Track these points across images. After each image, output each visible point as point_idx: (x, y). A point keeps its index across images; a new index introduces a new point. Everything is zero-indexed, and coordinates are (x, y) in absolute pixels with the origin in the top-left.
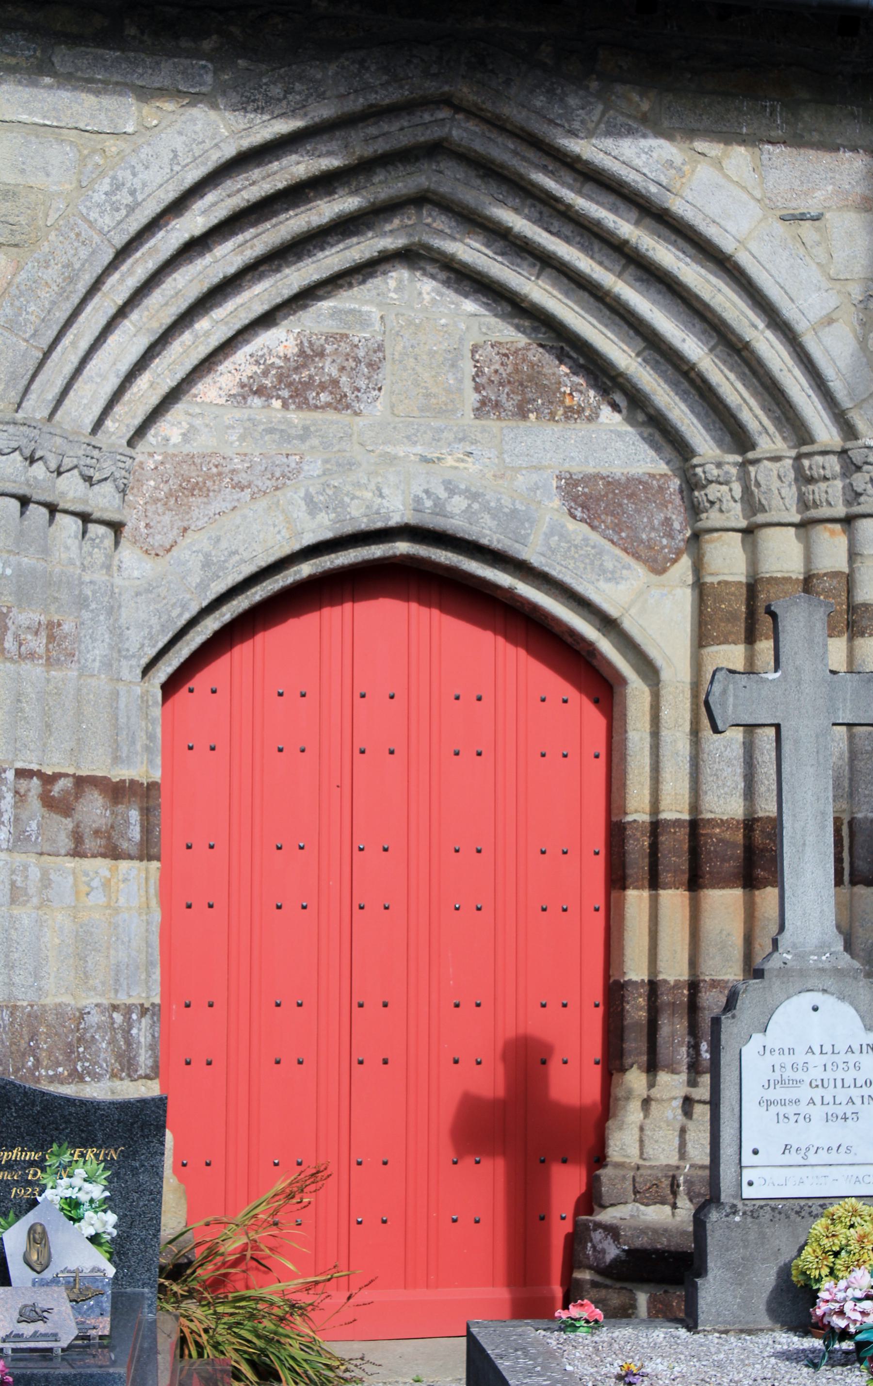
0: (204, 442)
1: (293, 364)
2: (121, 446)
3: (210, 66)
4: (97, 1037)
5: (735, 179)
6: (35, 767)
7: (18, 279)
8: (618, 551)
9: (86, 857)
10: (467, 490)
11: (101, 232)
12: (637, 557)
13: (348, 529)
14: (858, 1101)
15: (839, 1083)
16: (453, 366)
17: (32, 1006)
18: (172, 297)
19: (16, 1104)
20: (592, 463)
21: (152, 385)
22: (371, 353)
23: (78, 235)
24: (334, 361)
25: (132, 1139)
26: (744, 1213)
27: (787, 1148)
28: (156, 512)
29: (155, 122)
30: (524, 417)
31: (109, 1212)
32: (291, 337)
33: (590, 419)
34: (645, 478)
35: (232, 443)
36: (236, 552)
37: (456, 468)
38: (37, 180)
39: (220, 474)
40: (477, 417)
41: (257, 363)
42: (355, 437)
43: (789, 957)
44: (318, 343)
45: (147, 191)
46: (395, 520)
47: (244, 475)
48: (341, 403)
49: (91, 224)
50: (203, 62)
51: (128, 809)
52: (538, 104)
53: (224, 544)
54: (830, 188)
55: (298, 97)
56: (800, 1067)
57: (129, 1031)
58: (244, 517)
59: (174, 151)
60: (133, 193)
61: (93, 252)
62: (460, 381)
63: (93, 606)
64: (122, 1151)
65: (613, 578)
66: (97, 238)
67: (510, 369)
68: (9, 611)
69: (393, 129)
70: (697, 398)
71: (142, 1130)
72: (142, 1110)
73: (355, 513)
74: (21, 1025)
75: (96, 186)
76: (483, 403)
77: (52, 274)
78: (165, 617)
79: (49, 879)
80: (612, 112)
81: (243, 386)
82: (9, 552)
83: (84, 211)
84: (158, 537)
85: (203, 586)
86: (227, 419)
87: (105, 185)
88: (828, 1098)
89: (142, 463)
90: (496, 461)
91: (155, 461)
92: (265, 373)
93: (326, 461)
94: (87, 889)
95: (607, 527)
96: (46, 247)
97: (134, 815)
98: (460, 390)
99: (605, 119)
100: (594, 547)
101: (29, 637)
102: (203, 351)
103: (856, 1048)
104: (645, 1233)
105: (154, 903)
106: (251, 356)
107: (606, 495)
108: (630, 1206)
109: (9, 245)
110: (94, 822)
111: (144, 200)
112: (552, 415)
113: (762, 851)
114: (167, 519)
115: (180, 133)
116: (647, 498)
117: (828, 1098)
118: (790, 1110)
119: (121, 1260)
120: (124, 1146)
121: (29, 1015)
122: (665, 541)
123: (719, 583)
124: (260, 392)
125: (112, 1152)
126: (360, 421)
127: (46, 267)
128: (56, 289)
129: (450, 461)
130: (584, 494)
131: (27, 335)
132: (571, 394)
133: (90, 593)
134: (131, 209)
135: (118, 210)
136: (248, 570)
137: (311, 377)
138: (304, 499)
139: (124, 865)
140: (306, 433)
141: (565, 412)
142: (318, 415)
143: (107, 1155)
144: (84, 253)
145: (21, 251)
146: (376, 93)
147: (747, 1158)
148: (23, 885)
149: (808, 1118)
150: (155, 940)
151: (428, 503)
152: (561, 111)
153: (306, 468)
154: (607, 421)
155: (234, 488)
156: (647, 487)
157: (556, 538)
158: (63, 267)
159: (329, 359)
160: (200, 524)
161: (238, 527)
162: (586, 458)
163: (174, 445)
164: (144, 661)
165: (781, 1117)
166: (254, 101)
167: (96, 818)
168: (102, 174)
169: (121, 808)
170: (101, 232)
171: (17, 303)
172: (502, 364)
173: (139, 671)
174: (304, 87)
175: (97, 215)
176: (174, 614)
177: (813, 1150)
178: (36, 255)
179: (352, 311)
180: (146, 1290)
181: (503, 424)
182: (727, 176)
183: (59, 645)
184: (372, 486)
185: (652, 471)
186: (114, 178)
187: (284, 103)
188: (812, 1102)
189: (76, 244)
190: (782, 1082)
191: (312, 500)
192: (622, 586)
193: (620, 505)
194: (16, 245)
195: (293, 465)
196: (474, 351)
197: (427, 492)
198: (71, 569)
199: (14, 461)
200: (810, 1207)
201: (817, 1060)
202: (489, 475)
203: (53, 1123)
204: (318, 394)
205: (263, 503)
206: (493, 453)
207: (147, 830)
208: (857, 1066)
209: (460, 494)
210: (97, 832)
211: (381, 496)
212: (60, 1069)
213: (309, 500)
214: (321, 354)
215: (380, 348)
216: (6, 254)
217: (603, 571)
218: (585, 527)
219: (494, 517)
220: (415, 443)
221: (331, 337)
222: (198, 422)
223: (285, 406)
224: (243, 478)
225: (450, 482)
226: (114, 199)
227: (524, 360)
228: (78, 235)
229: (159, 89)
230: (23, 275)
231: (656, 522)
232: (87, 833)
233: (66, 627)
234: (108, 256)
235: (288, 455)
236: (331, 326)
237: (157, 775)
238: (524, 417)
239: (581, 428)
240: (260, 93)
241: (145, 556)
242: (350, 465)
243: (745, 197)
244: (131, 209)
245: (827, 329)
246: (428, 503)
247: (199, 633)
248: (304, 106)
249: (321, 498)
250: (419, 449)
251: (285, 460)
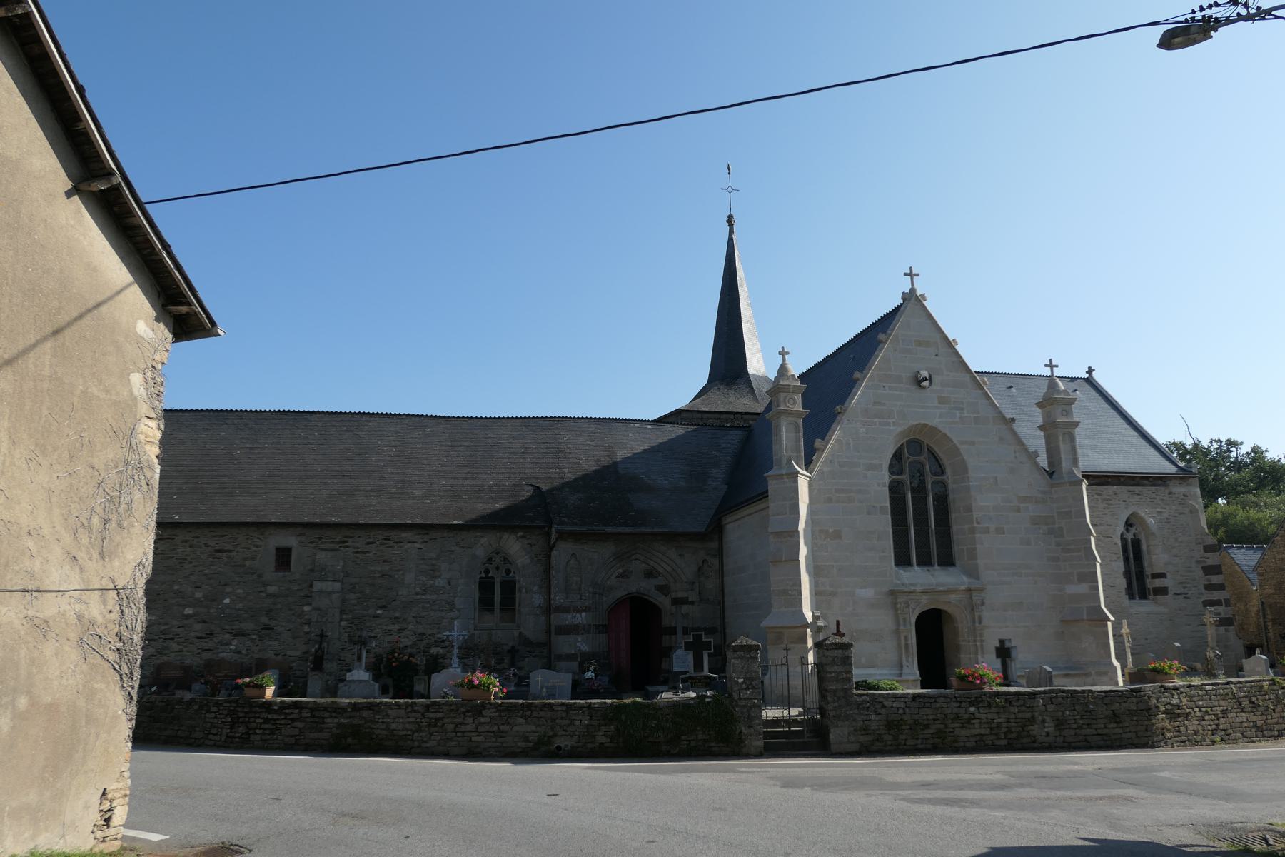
48: (628, 578)
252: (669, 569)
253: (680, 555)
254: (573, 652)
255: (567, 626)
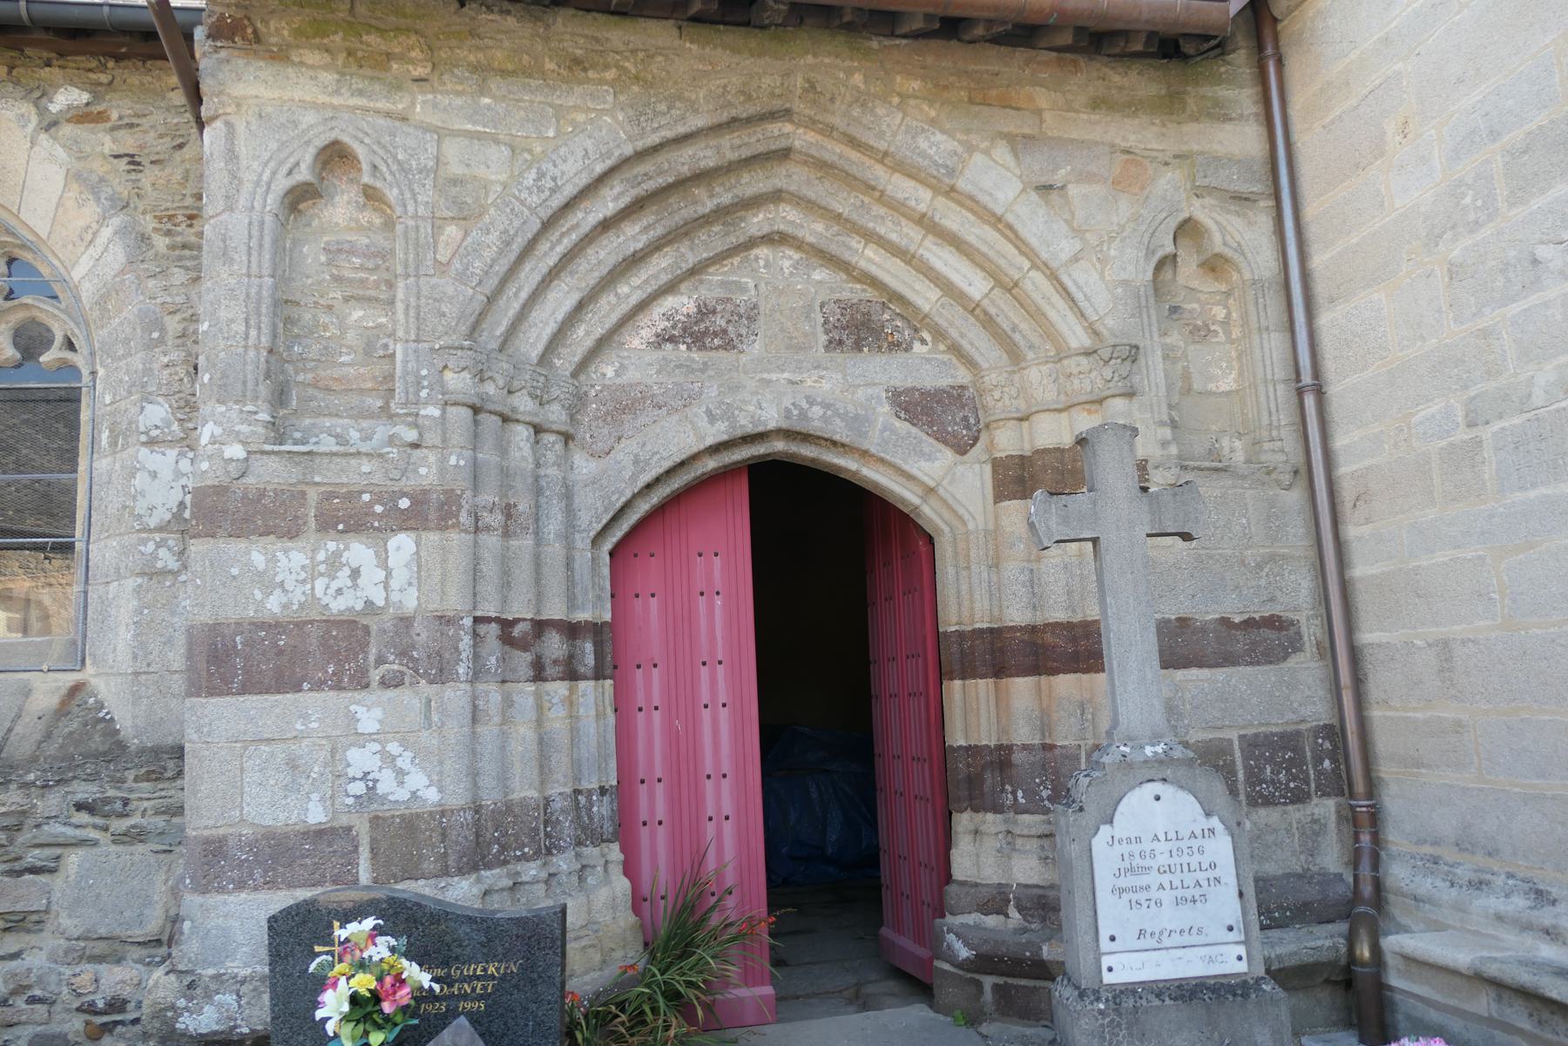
0: (632, 375)
1: (694, 320)
7: (465, 244)
8: (932, 440)
11: (529, 208)
12: (945, 442)
13: (739, 433)
14: (1205, 883)
15: (1185, 868)
19: (422, 924)
23: (512, 210)
26: (1107, 1000)
27: (1142, 933)
28: (597, 427)
30: (861, 350)
33: (906, 350)
36: (658, 452)
38: (481, 171)
41: (668, 320)
43: (1127, 750)
45: (565, 178)
46: (772, 425)
48: (728, 345)
49: (522, 203)
53: (648, 447)
54: (1069, 168)
58: (662, 427)
59: (586, 150)
60: (554, 179)
61: (524, 223)
63: (548, 493)
65: (930, 458)
66: (526, 212)
67: (848, 317)
73: (743, 422)
77: (493, 237)
78: (606, 502)
85: (634, 478)
86: (647, 359)
87: (533, 174)
88: (1177, 883)
92: (674, 327)
93: (720, 386)
94: (549, 705)
96: (487, 219)
97: (589, 647)
98: (814, 334)
102: (625, 308)
103: (1198, 832)
105: (610, 711)
108: (973, 915)
112: (880, 348)
117: (1177, 883)
118: (1142, 896)
121: (493, 811)
124: (672, 339)
129: (810, 383)
136: (667, 465)
137: (706, 328)
138: (706, 412)
140: (705, 367)
142: (713, 354)
144: (516, 223)
147: (1105, 944)
151: (795, 412)
164: (592, 534)
168: (529, 168)
169: (578, 642)
170: (529, 208)
176: (614, 498)
186: (538, 169)
188: (1161, 887)
190: (1131, 870)
192: (937, 464)
193: (932, 408)
194: (464, 219)
196: (822, 306)
197: (793, 404)
198: (524, 464)
199: (464, 379)
201: (1162, 847)
202: (837, 392)
205: (676, 417)
206: (839, 376)
208: (1201, 851)
210: (555, 662)
211: (761, 408)
212: (526, 850)
213: (709, 413)
215: (755, 306)
217: (922, 454)
219: (842, 420)
220: (783, 371)
221: (720, 300)
223: (689, 348)
224: (660, 400)
230: (469, 239)
232: (547, 662)
233: (520, 508)
234: (535, 225)
236: (720, 293)
238: (861, 350)
239: (900, 356)
243: (1009, 175)
244: (553, 191)
246: (795, 412)
250: (786, 375)
252: (976, 285)
253: (1045, 189)
254: (316, 815)
255: (275, 627)
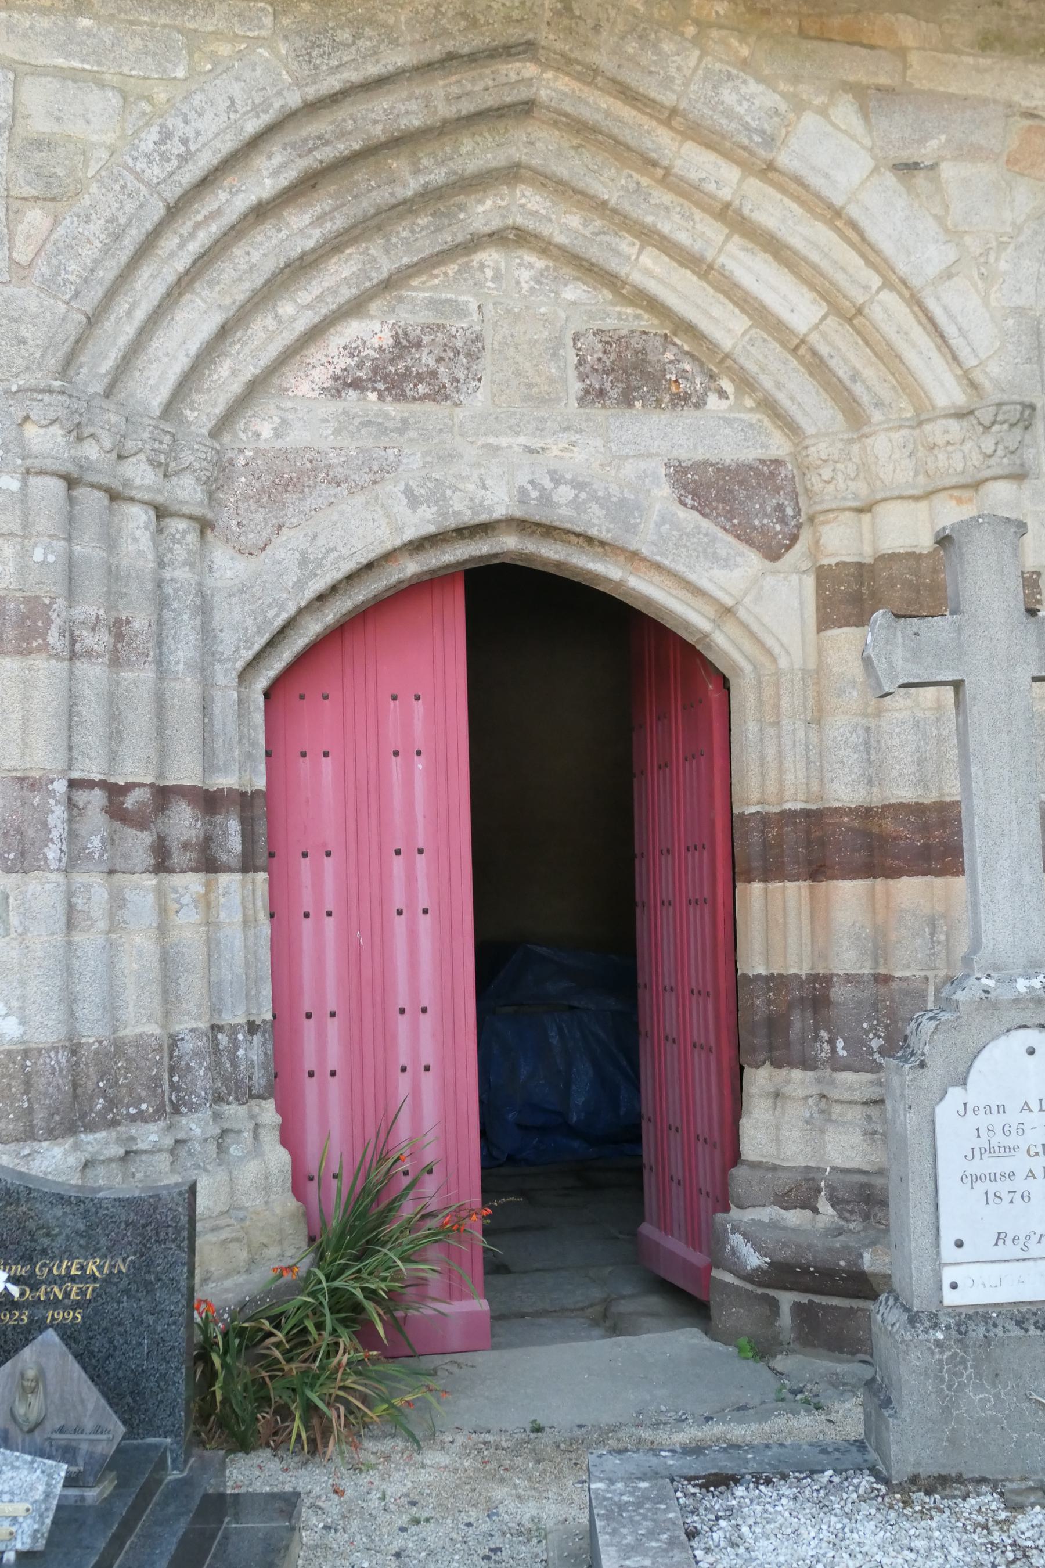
0: (297, 437)
1: (389, 356)
2: (202, 435)
3: (269, 8)
4: (193, 1064)
5: (843, 127)
6: (97, 777)
7: (54, 236)
8: (730, 538)
9: (175, 872)
10: (572, 481)
11: (148, 184)
12: (750, 542)
13: (452, 523)
16: (554, 354)
17: (100, 1042)
18: (245, 272)
20: (700, 451)
21: (234, 373)
22: (469, 343)
23: (123, 187)
24: (431, 352)
25: (145, 1245)
27: (1000, 1237)
28: (248, 510)
29: (209, 67)
30: (630, 405)
31: (925, 543)
32: (386, 329)
33: (697, 406)
34: (756, 464)
35: (326, 437)
36: (335, 549)
37: (562, 458)
39: (313, 469)
40: (580, 406)
41: (351, 355)
42: (456, 428)
44: (414, 334)
45: (202, 140)
46: (500, 512)
47: (341, 470)
48: (438, 395)
49: (138, 176)
50: (262, 5)
51: (226, 818)
52: (631, 51)
53: (321, 541)
54: (943, 137)
55: (368, 43)
56: (1013, 1130)
57: (235, 1053)
60: (185, 142)
61: (141, 206)
62: (564, 370)
63: (176, 605)
64: (132, 1262)
65: (726, 564)
66: (144, 191)
67: (613, 356)
68: (52, 603)
69: (476, 89)
70: (807, 376)
71: (157, 1234)
72: (156, 1208)
73: (458, 507)
74: (87, 1064)
75: (143, 135)
76: (587, 392)
77: (96, 228)
78: (260, 619)
79: (124, 899)
80: (709, 58)
81: (336, 378)
82: (50, 536)
83: (130, 162)
84: (251, 536)
85: (300, 585)
89: (232, 459)
90: (602, 450)
91: (246, 458)
92: (360, 366)
95: (719, 515)
96: (86, 201)
97: (234, 826)
99: (703, 65)
100: (706, 535)
101: (85, 633)
104: (789, 1247)
106: (345, 348)
107: (717, 482)
109: (45, 199)
110: (182, 834)
111: (198, 150)
112: (659, 402)
113: (895, 839)
114: (259, 517)
115: (237, 79)
116: (758, 484)
118: (1003, 1187)
119: (135, 1401)
120: (135, 1254)
122: (778, 527)
123: (837, 564)
124: (356, 384)
125: (120, 1262)
126: (460, 414)
127: (87, 222)
128: (99, 245)
129: (555, 451)
130: (694, 481)
131: (67, 297)
132: (676, 381)
133: (171, 592)
134: (184, 159)
135: (169, 160)
136: (348, 567)
137: (407, 368)
139: (224, 879)
140: (404, 426)
141: (672, 400)
142: (416, 407)
143: (114, 1266)
144: (129, 207)
145: (59, 205)
146: (454, 39)
148: (86, 908)
149: (1027, 1197)
150: (265, 955)
151: (534, 494)
152: (654, 58)
153: (405, 461)
154: (715, 408)
155: (329, 483)
156: (758, 473)
157: (667, 526)
158: (107, 221)
159: (426, 350)
160: (295, 521)
161: (335, 523)
162: (695, 445)
163: (266, 440)
164: (240, 665)
165: (991, 1196)
166: (319, 46)
167: (184, 831)
168: (148, 124)
170: (148, 184)
171: (54, 262)
172: (605, 352)
173: (234, 675)
174: (375, 33)
175: (144, 166)
176: (271, 613)
177: (1035, 1239)
178: (75, 209)
179: (449, 301)
180: (169, 1440)
181: (609, 412)
182: (834, 125)
183: (128, 644)
184: (475, 478)
185: (762, 457)
186: (162, 126)
187: (353, 49)
188: (1031, 1174)
189: (121, 197)
190: (990, 1150)
191: (413, 494)
192: (737, 573)
193: (731, 491)
194: (53, 199)
195: (392, 458)
197: (531, 482)
198: (141, 562)
200: (1035, 1314)
203: (43, 1227)
204: (416, 385)
205: (360, 498)
206: (599, 442)
207: (248, 837)
209: (566, 483)
210: (186, 846)
211: (484, 487)
212: (144, 1106)
213: (409, 493)
214: (418, 345)
215: (478, 338)
216: (42, 209)
217: (715, 558)
218: (696, 514)
219: (602, 507)
220: (517, 434)
222: (290, 417)
223: (381, 398)
224: (339, 472)
225: (555, 472)
226: (164, 148)
227: (627, 348)
228: (123, 187)
229: (213, 33)
230: (61, 230)
231: (769, 510)
232: (174, 846)
234: (157, 211)
235: (385, 448)
237: (260, 783)
238: (630, 405)
239: (688, 415)
240: (326, 38)
241: (238, 556)
242: (449, 457)
243: (855, 146)
244: (184, 159)
245: (947, 284)
246: (534, 494)
247: (302, 636)
248: (375, 53)
249: (423, 491)
250: (522, 440)
251: (383, 453)
